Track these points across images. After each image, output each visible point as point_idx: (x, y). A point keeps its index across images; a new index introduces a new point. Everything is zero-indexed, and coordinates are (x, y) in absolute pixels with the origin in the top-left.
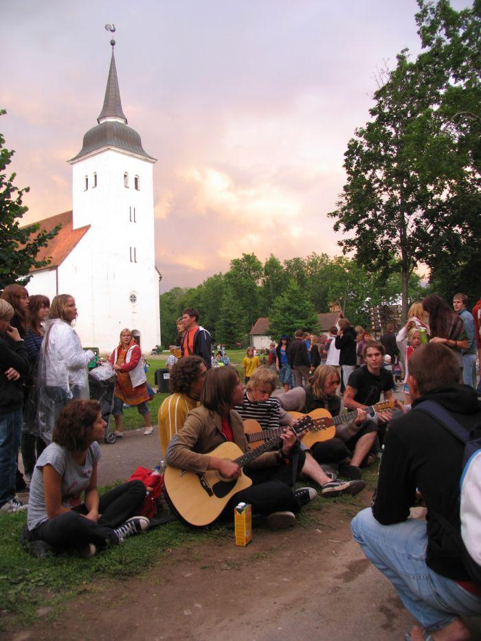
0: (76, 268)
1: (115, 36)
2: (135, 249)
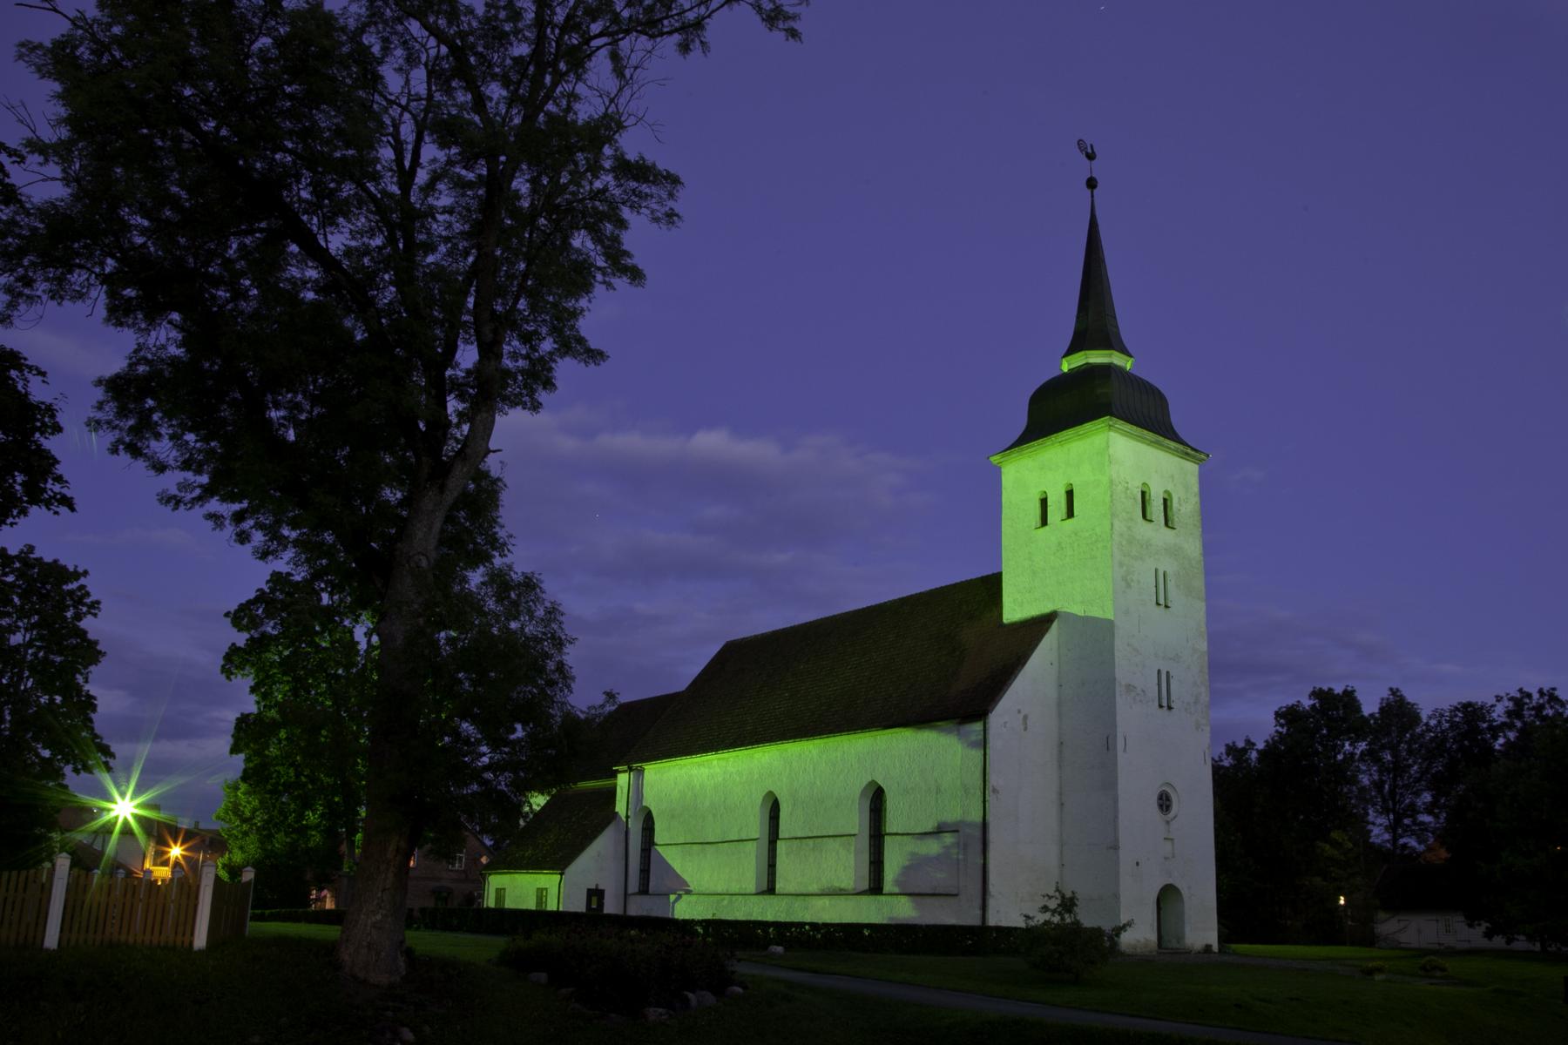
0: (1025, 717)
1: (1098, 169)
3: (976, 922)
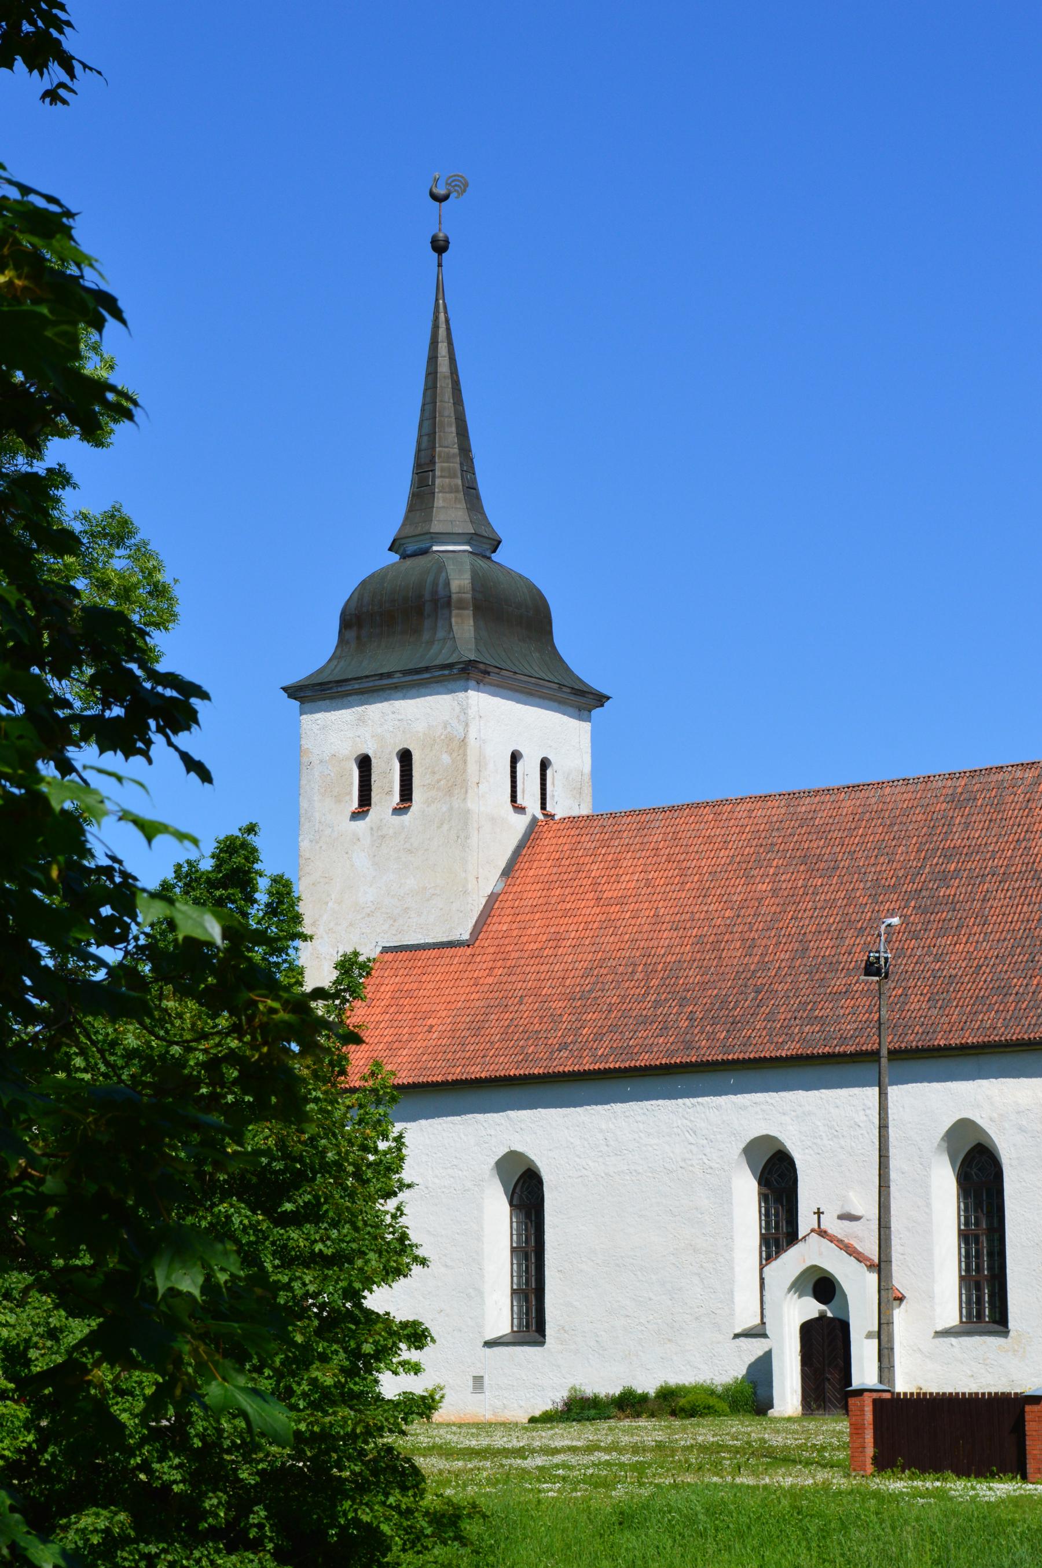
1: (451, 220)
2: (544, 765)
3: (894, 1092)
